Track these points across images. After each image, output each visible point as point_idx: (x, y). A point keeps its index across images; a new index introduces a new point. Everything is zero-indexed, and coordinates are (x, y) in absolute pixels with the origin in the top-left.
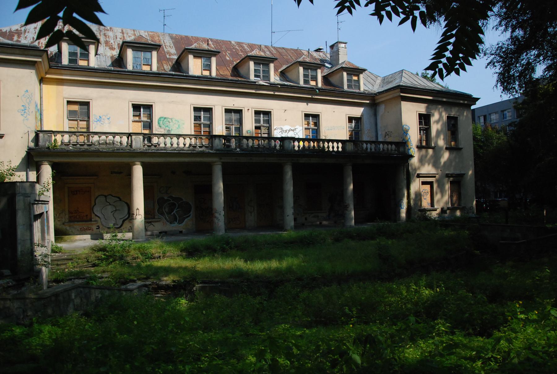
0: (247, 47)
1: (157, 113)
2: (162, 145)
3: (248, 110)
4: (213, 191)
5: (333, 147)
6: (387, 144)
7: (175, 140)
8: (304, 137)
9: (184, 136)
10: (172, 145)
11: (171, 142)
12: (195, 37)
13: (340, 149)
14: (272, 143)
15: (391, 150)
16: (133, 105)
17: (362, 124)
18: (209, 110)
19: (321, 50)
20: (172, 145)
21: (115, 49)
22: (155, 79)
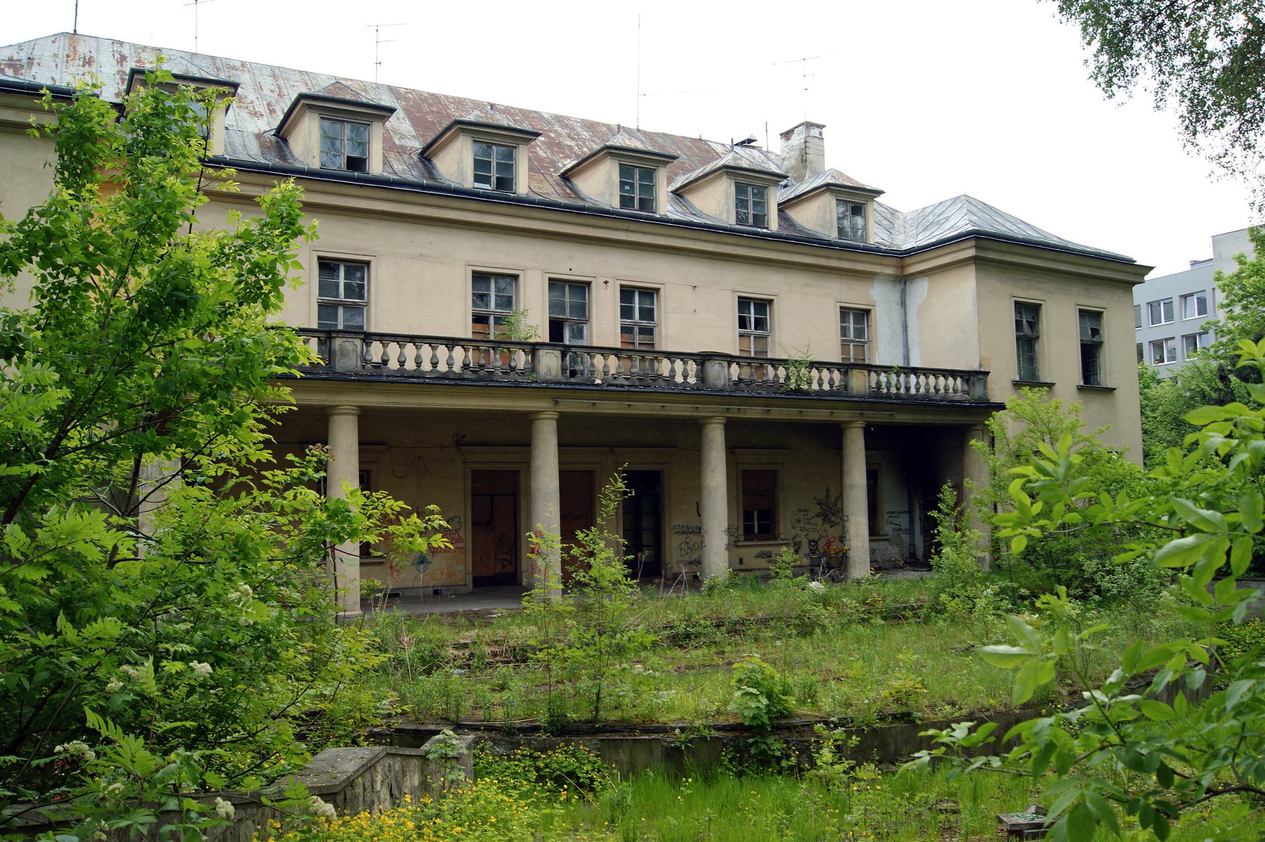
0: (582, 127)
1: (381, 282)
2: (393, 365)
3: (606, 282)
4: (533, 485)
5: (820, 383)
6: (924, 374)
7: (442, 351)
8: (840, 361)
9: (451, 342)
10: (435, 364)
11: (434, 356)
12: (453, 98)
13: (692, 380)
14: (519, 358)
15: (955, 391)
16: (320, 258)
17: (873, 327)
18: (581, 287)
19: (752, 144)
20: (435, 364)
21: (262, 115)
22: (383, 194)
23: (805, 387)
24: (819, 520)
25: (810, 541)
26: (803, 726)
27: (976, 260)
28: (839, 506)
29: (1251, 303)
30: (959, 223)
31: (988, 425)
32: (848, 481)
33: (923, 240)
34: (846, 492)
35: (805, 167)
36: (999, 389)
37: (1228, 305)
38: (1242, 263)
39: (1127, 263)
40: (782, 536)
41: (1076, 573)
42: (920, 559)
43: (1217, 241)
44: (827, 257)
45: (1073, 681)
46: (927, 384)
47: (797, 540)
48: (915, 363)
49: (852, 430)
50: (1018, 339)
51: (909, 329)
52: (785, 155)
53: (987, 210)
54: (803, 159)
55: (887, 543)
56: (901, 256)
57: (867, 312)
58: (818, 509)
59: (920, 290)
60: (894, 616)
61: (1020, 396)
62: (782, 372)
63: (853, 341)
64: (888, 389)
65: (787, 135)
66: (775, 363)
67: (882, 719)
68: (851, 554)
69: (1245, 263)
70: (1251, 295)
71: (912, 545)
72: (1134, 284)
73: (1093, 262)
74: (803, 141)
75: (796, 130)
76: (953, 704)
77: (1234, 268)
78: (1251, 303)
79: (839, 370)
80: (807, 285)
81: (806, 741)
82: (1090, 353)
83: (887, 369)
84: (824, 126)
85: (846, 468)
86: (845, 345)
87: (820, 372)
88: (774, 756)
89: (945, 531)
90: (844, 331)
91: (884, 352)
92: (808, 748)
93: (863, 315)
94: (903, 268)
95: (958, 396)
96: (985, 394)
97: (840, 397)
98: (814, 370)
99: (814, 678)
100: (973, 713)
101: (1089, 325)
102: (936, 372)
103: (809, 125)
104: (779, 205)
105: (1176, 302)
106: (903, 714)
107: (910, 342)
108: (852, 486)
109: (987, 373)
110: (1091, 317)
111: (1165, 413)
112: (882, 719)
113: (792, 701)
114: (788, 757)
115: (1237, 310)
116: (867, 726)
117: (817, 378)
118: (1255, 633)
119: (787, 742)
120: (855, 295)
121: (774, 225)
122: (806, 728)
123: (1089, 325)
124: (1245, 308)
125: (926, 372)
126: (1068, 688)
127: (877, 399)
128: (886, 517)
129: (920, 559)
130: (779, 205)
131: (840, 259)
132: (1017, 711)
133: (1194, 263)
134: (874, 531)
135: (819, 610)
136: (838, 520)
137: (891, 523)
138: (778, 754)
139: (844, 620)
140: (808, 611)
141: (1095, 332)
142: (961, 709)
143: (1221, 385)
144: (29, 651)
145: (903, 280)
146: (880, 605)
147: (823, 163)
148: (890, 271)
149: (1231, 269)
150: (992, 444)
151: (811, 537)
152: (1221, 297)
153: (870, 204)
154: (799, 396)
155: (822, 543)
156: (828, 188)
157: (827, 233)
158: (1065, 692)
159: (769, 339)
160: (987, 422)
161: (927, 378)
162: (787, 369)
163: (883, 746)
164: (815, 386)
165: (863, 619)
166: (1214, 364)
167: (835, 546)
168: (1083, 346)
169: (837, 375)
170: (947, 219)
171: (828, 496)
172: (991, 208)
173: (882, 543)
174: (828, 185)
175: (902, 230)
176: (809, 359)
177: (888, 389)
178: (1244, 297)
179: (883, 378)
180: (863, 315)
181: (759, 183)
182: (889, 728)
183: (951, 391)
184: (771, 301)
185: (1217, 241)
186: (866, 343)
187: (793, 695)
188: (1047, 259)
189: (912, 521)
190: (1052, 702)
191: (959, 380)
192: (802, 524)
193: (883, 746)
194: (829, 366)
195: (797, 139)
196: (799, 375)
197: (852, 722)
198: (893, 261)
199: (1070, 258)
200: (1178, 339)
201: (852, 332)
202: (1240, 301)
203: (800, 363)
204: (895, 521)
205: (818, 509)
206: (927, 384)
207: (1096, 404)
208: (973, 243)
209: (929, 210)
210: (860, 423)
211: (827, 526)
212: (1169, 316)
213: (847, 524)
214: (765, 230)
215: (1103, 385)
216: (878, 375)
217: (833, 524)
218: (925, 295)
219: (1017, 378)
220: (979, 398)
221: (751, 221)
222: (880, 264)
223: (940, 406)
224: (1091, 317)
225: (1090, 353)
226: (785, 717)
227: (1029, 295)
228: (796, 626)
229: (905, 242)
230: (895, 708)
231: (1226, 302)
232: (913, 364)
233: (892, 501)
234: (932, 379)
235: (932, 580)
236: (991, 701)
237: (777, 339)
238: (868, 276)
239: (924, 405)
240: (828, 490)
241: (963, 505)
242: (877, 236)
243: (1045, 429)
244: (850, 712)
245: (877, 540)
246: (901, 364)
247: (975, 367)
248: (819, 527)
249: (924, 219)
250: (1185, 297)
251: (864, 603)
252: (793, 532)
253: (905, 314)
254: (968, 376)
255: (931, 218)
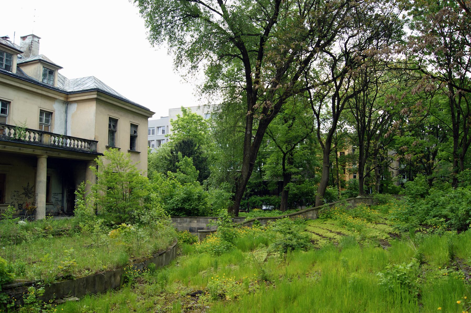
6: (73, 140)
17: (53, 119)
23: (22, 139)
24: (24, 196)
25: (19, 205)
26: (19, 286)
27: (96, 99)
28: (33, 190)
29: (180, 130)
30: (90, 85)
31: (96, 161)
32: (38, 179)
33: (76, 89)
34: (37, 184)
35: (30, 52)
36: (101, 148)
37: (174, 130)
38: (179, 117)
39: (147, 110)
40: (6, 202)
41: (128, 216)
42: (70, 212)
43: (170, 111)
44: (37, 89)
45: (134, 256)
46: (74, 143)
47: (13, 204)
48: (69, 134)
49: (42, 158)
50: (109, 131)
51: (68, 122)
52: (22, 46)
53: (101, 84)
54: (30, 49)
55: (52, 206)
56: (68, 94)
57: (51, 113)
58: (23, 191)
59: (73, 108)
60: (58, 234)
61: (108, 151)
62: (12, 131)
63: (44, 124)
64: (58, 143)
65: (24, 38)
66: (10, 127)
67: (57, 279)
68: (38, 210)
69: (179, 118)
70: (181, 128)
71: (62, 206)
72: (149, 117)
73: (137, 108)
74: (30, 42)
75: (28, 37)
76: (88, 269)
77: (176, 119)
78: (180, 130)
79: (38, 133)
80: (27, 98)
81: (20, 294)
82: (133, 139)
83: (58, 136)
84: (40, 38)
85: (38, 174)
86: (41, 125)
87: (30, 133)
88: (3, 303)
89: (78, 201)
90: (41, 120)
91: (57, 128)
92: (21, 297)
93: (49, 114)
94: (67, 98)
95: (86, 149)
96: (96, 149)
97: (38, 145)
98: (27, 132)
99: (24, 263)
100: (97, 272)
101: (133, 129)
102: (78, 139)
103: (34, 36)
104: (17, 64)
105: (156, 129)
106: (67, 277)
107: (67, 127)
108: (40, 182)
109: (97, 142)
110: (134, 127)
111: (153, 163)
112: (57, 279)
113: (13, 275)
114: (10, 303)
115: (176, 132)
116: (51, 283)
117: (29, 135)
118: (186, 235)
119: (10, 295)
120: (47, 106)
121: (14, 71)
122: (20, 287)
123: (133, 129)
124: (178, 132)
125: (74, 139)
126: (133, 259)
127: (52, 148)
128: (52, 195)
129: (70, 212)
130: (17, 64)
131: (42, 90)
132: (114, 270)
133: (162, 117)
134: (47, 201)
135: (24, 232)
136: (32, 196)
137: (54, 198)
138: (5, 302)
139: (35, 237)
140: (19, 233)
141: (135, 132)
142: (92, 271)
143: (171, 155)
144: (280, 262)
145: (67, 103)
146: (52, 230)
147: (38, 52)
148: (62, 99)
149: (175, 119)
150: (97, 168)
151: (19, 203)
152: (171, 127)
153: (56, 71)
154: (19, 142)
155: (24, 206)
156: (40, 61)
157: (38, 79)
158: (132, 261)
159: (7, 118)
160: (95, 160)
161: (74, 141)
162: (15, 130)
163: (58, 291)
164: (27, 139)
165: (44, 236)
166: (169, 149)
167: (30, 206)
168: (131, 136)
169: (37, 136)
170: (86, 83)
171: (28, 186)
172: (102, 83)
173: (50, 206)
174: (40, 60)
175: (68, 85)
176: (25, 127)
177: (58, 143)
178: (179, 128)
179: (57, 139)
180: (49, 114)
181: (9, 52)
182: (61, 283)
183: (83, 147)
184: (10, 102)
185: (170, 111)
186: (49, 125)
187: (13, 272)
188: (122, 104)
189: (63, 197)
190: (128, 265)
191: (86, 143)
192: (16, 197)
193: (58, 291)
194: (34, 131)
195: (28, 41)
196: (20, 133)
197: (43, 282)
198: (64, 95)
199: (129, 105)
200: (155, 141)
201: (44, 120)
202: (177, 129)
203: (21, 128)
204: (56, 197)
205: (23, 191)
206: (74, 143)
207: (134, 157)
208: (96, 93)
209: (79, 80)
210: (46, 156)
211: (27, 198)
212: (153, 133)
213: (37, 197)
214: (10, 72)
215: (136, 151)
216: (55, 137)
217: (30, 198)
218: (75, 110)
219: (108, 145)
220: (94, 151)
221: (4, 67)
222: (59, 96)
223: (79, 152)
224: (134, 127)
225: (133, 139)
226: (9, 283)
227: (115, 115)
228: (13, 240)
229: (69, 89)
230: (62, 274)
231: (173, 129)
232: (68, 135)
233: (56, 189)
234: (76, 142)
235: (73, 219)
236: (104, 267)
237: (11, 119)
238: (53, 99)
239: (72, 151)
240: (28, 183)
241: (86, 192)
242: (58, 85)
243: (118, 163)
244: (43, 278)
245: (48, 204)
246: (64, 134)
247: (93, 139)
248: (23, 199)
249: (76, 82)
250: (158, 128)
251: (44, 229)
252: (12, 201)
253: (67, 116)
254: (90, 142)
255: (80, 82)
